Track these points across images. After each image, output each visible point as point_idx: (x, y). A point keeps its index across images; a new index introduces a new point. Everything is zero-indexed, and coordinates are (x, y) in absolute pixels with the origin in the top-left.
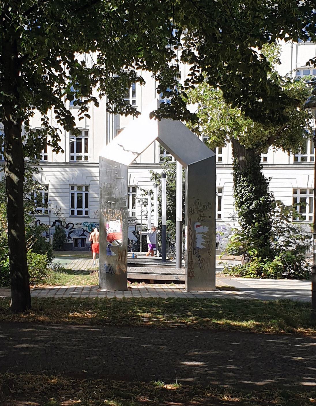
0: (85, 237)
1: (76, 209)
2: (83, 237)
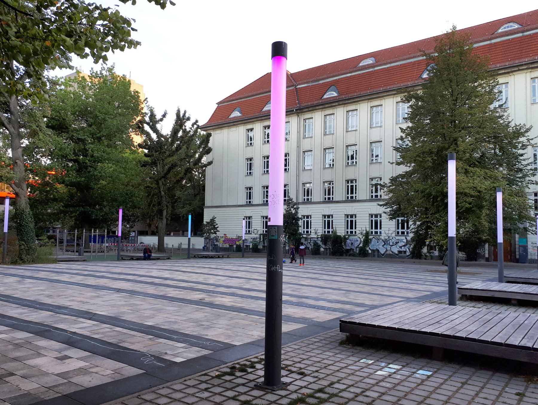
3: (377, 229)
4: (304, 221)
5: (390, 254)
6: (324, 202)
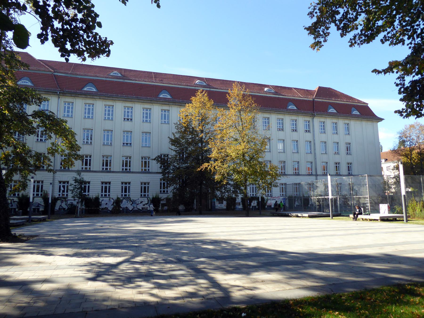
0: (39, 208)
1: (143, 194)
2: (38, 207)
3: (126, 192)
4: (250, 187)
5: (136, 210)
6: (122, 172)
